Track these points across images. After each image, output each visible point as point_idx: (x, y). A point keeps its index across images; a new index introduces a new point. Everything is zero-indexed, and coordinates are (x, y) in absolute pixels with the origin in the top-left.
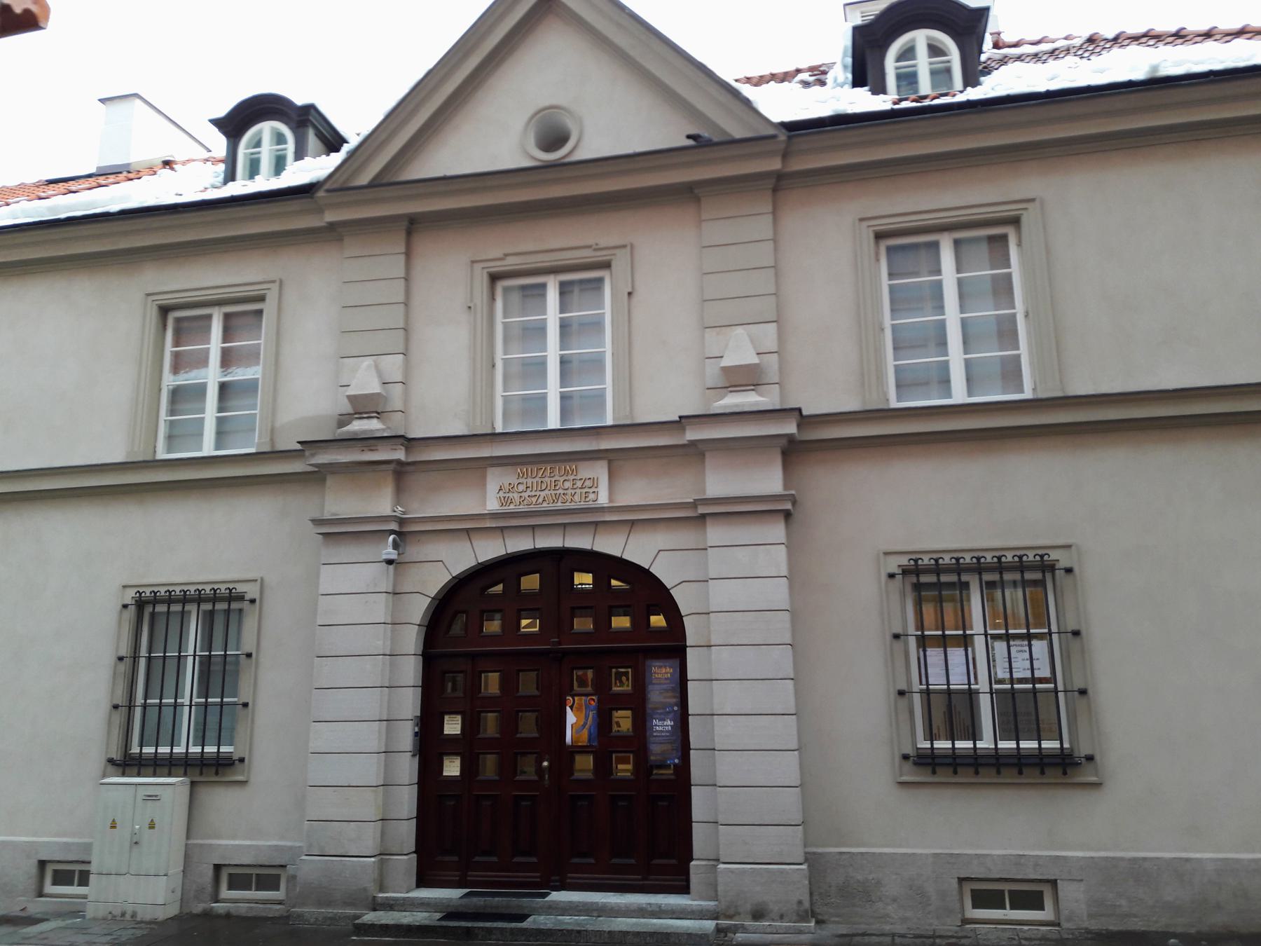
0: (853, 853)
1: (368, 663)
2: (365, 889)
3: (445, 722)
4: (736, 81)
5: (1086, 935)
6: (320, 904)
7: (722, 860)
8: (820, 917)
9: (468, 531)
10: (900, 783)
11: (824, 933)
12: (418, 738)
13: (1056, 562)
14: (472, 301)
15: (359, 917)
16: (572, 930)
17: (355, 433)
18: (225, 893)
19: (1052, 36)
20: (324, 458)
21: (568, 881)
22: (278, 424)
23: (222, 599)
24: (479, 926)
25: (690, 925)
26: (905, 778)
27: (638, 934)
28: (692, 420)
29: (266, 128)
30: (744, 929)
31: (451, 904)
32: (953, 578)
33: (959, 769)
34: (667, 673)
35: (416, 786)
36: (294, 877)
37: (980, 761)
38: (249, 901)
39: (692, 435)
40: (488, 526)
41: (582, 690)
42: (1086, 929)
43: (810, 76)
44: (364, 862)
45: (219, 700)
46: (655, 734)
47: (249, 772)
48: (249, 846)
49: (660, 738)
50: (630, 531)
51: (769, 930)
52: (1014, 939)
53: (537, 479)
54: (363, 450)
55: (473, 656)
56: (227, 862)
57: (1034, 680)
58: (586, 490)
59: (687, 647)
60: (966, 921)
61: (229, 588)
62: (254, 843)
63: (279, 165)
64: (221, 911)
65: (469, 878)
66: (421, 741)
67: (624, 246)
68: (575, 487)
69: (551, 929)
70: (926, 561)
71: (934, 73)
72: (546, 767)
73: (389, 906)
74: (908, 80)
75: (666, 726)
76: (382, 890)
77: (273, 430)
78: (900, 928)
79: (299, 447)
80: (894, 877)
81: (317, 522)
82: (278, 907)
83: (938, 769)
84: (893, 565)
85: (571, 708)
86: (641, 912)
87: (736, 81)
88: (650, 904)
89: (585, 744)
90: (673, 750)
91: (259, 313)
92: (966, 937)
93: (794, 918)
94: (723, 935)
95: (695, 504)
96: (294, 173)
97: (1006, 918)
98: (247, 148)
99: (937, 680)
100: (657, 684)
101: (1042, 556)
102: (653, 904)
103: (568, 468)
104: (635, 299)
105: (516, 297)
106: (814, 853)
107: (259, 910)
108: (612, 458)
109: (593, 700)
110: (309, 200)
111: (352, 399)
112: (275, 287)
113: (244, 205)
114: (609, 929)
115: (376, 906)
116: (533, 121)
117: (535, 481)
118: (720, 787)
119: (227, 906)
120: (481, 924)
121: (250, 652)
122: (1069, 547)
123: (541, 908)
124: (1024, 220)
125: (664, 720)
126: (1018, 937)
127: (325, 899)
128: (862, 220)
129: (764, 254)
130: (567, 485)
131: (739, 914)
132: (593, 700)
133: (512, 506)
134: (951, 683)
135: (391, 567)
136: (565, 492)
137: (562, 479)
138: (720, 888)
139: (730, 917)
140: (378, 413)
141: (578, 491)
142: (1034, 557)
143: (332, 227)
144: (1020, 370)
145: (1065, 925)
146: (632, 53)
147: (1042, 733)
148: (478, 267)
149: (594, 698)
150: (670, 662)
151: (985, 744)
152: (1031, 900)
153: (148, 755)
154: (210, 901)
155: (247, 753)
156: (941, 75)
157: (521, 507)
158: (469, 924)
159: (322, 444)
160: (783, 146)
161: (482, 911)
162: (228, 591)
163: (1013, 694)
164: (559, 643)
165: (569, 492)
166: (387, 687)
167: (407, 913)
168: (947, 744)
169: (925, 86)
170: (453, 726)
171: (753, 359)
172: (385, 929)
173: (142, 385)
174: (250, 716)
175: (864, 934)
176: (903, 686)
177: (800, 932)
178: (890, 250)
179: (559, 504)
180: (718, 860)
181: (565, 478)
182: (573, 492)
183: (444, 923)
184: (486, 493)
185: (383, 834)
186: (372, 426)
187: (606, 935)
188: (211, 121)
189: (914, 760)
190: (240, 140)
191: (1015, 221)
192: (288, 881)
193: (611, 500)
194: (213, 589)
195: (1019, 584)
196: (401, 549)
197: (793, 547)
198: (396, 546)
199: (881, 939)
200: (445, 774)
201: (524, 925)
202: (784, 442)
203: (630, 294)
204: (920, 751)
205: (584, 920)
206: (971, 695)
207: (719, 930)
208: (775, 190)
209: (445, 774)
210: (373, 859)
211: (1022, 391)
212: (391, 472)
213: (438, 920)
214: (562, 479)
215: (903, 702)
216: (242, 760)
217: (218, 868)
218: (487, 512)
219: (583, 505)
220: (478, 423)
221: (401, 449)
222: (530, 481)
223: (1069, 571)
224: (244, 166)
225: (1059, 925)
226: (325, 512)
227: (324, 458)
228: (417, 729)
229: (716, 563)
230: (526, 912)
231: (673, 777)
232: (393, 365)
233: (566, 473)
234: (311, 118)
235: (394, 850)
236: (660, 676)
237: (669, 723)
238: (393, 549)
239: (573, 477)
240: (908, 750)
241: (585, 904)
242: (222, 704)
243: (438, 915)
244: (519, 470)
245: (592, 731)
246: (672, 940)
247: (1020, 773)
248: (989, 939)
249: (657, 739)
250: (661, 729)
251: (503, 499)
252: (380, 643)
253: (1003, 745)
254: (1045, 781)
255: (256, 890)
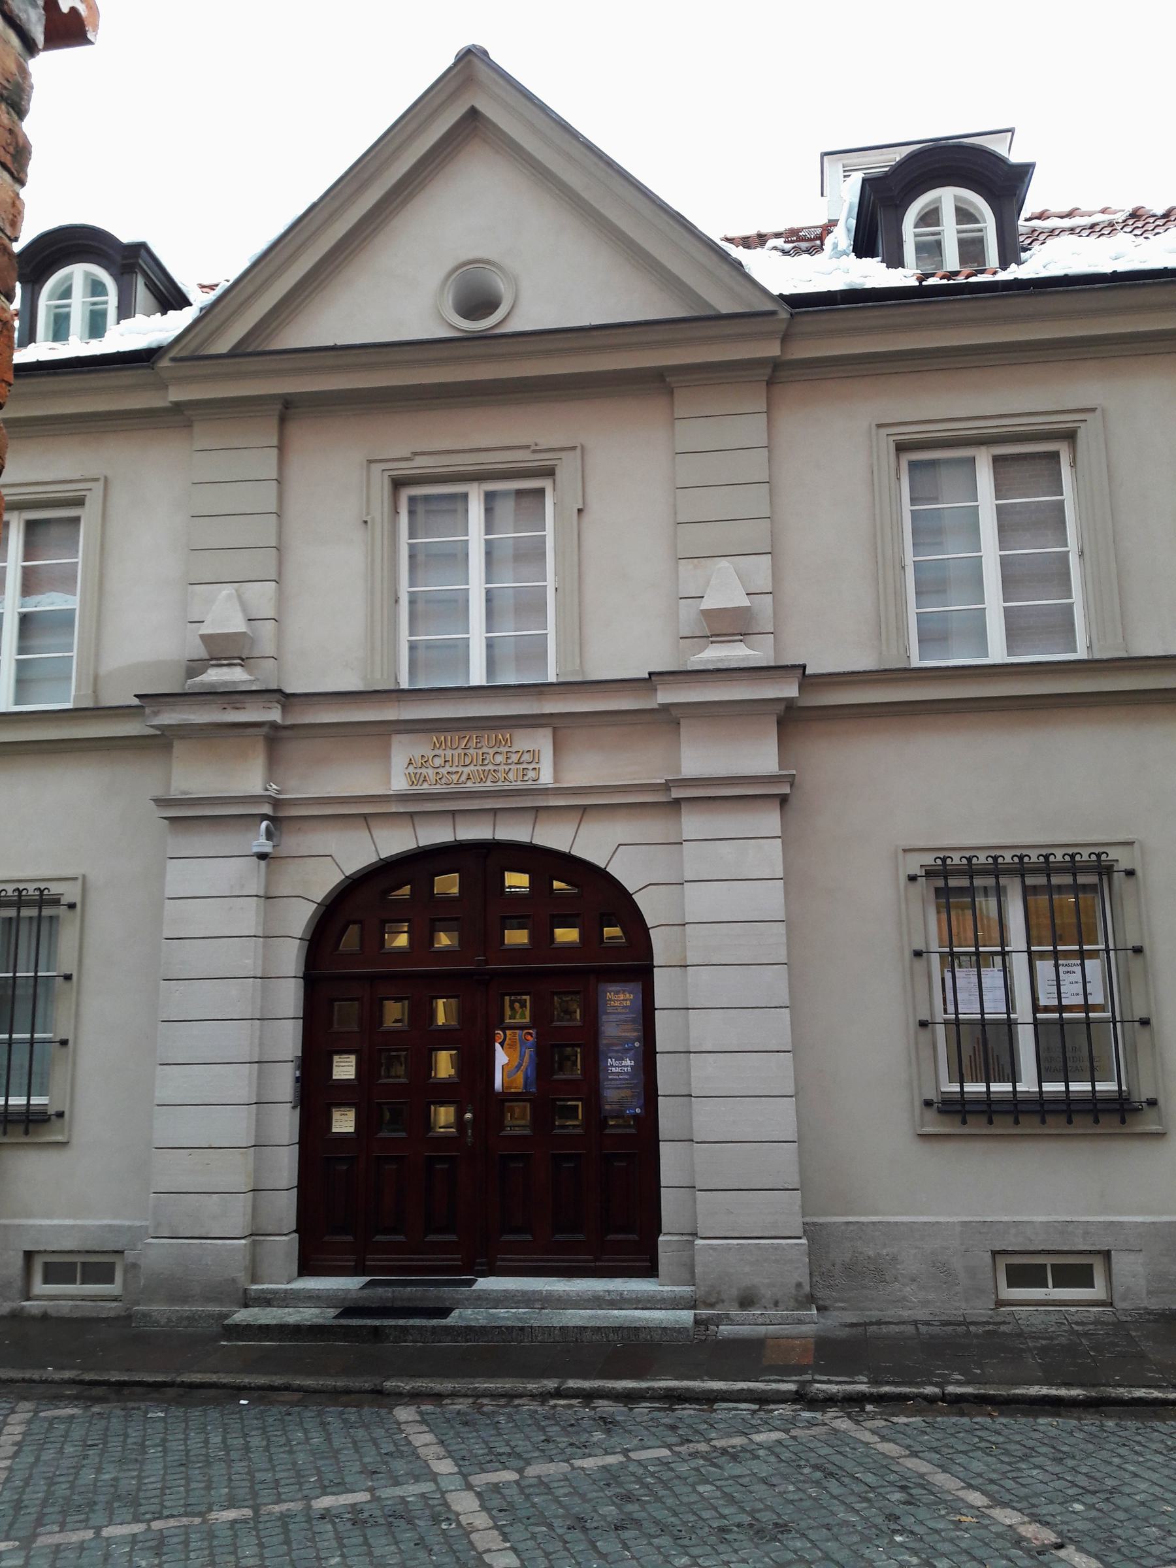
0: (863, 1223)
1: (233, 988)
2: (234, 1280)
3: (335, 1064)
4: (728, 240)
5: (1147, 1317)
6: (172, 1299)
7: (700, 1234)
8: (821, 1303)
9: (365, 817)
10: (920, 1135)
11: (829, 1322)
12: (299, 1084)
13: (1115, 864)
14: (368, 514)
15: (227, 1316)
16: (513, 1327)
17: (212, 685)
18: (40, 1287)
19: (1084, 208)
20: (170, 717)
21: (499, 1263)
22: (103, 670)
23: (30, 903)
24: (390, 1324)
25: (662, 1317)
26: (929, 1130)
27: (598, 1329)
28: (666, 678)
29: (78, 273)
30: (729, 1320)
31: (349, 1296)
32: (964, 882)
33: (969, 1118)
34: (626, 1000)
35: (297, 1146)
36: (135, 1266)
37: (1020, 1107)
38: (72, 1298)
39: (665, 696)
40: (394, 810)
41: (518, 1020)
42: (1146, 1308)
43: (785, 242)
44: (232, 1245)
45: (28, 1036)
46: (610, 1077)
47: (70, 1130)
48: (73, 1227)
49: (618, 1082)
50: (536, 818)
51: (760, 1321)
52: (1064, 1324)
53: (459, 751)
54: (225, 708)
55: (373, 978)
56: (42, 1248)
57: (1061, 1008)
58: (525, 766)
59: (655, 967)
60: (1000, 1303)
61: (39, 889)
62: (79, 1222)
63: (96, 327)
64: (35, 1312)
65: (499, 1263)
66: (302, 1086)
67: (574, 448)
68: (509, 761)
69: (485, 1327)
70: (956, 861)
71: (962, 243)
72: (469, 1121)
73: (266, 1300)
74: (931, 249)
75: (625, 1066)
76: (254, 1280)
77: (96, 678)
78: (921, 1314)
79: (136, 702)
80: (913, 1251)
81: (161, 802)
82: (114, 1304)
83: (995, 1118)
84: (913, 866)
85: (502, 1044)
86: (597, 1301)
87: (728, 240)
88: (607, 1291)
89: (520, 1091)
90: (633, 1096)
91: (76, 520)
92: (1004, 1323)
93: (792, 1304)
94: (703, 1328)
95: (667, 786)
96: (122, 335)
97: (1047, 1298)
98: (50, 298)
99: (969, 1009)
100: (614, 1013)
101: (1098, 855)
102: (613, 1291)
103: (500, 737)
104: (587, 518)
105: (506, 508)
106: (814, 1224)
107: (88, 1309)
108: (556, 724)
109: (531, 1034)
110: (150, 371)
111: (207, 639)
112: (98, 487)
113: (56, 374)
114: (561, 1325)
115: (247, 1301)
116: (450, 282)
117: (456, 753)
118: (697, 1143)
119: (44, 1305)
120: (392, 1322)
121: (69, 973)
122: (1131, 844)
123: (467, 1300)
124: (1081, 435)
125: (623, 1060)
126: (1068, 1321)
127: (177, 1291)
128: (879, 426)
129: (754, 466)
130: (499, 759)
131: (723, 1301)
132: (531, 1034)
133: (425, 786)
134: (986, 1011)
135: (263, 863)
136: (496, 768)
137: (491, 751)
138: (698, 1270)
139: (711, 1306)
140: (242, 660)
141: (513, 767)
142: (1038, 858)
143: (178, 408)
144: (1073, 624)
145: (1120, 1305)
146: (586, 195)
147: (1096, 1074)
148: (377, 468)
149: (531, 1031)
150: (632, 985)
151: (1027, 1084)
152: (1078, 1275)
153: (16, 1108)
154: (19, 1298)
155: (68, 1105)
156: (971, 250)
157: (438, 786)
158: (377, 1322)
159: (167, 699)
160: (783, 326)
161: (389, 1305)
162: (37, 893)
163: (1062, 1025)
164: (486, 962)
165: (501, 768)
166: (258, 1019)
167: (291, 1310)
168: (981, 1087)
169: (951, 259)
170: (344, 1069)
171: (745, 602)
172: (265, 1331)
173: (378, 573)
174: (70, 1059)
175: (879, 1323)
176: (925, 1016)
177: (800, 1322)
178: (913, 465)
179: (489, 783)
180: (695, 1234)
181: (496, 749)
182: (507, 768)
183: (343, 1322)
184: (390, 763)
185: (255, 1208)
186: (235, 676)
187: (556, 1332)
188: (955, 196)
189: (938, 1107)
190: (41, 288)
191: (1070, 436)
192: (126, 1272)
193: (556, 781)
194: (18, 889)
195: (992, 892)
196: (275, 839)
197: (787, 838)
198: (269, 835)
199: (902, 1328)
200: (334, 1130)
201: (449, 1321)
202: (782, 707)
203: (580, 511)
204: (945, 1096)
205: (524, 1313)
206: (1010, 1025)
207: (697, 1322)
208: (770, 383)
209: (334, 1130)
210: (243, 1241)
211: (1075, 651)
212: (262, 737)
213: (334, 1318)
214: (491, 751)
215: (925, 1035)
216: (60, 1115)
217: (29, 1255)
218: (392, 792)
219: (519, 785)
220: (378, 676)
221: (277, 708)
222: (449, 753)
223: (1130, 873)
224: (47, 325)
225: (1111, 1305)
226: (172, 789)
227: (170, 717)
228: (298, 1074)
229: (694, 861)
230: (447, 1304)
231: (527, 1132)
232: (262, 596)
233: (498, 743)
234: (140, 261)
235: (270, 1230)
236: (617, 1004)
237: (628, 1062)
238: (267, 840)
239: (507, 749)
240: (931, 1095)
241: (524, 1293)
242: (32, 1042)
243: (332, 1312)
244: (435, 738)
245: (529, 1073)
246: (642, 1336)
247: (1096, 1121)
248: (1033, 1325)
249: (613, 1082)
250: (618, 1070)
251: (413, 776)
252: (249, 962)
253: (1048, 1087)
254: (1098, 1131)
255: (82, 1283)
